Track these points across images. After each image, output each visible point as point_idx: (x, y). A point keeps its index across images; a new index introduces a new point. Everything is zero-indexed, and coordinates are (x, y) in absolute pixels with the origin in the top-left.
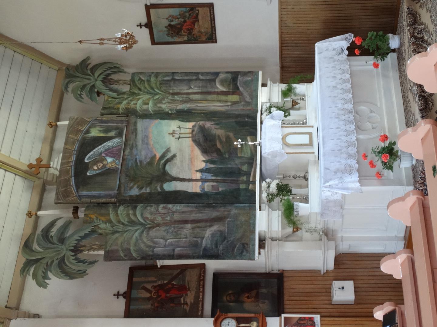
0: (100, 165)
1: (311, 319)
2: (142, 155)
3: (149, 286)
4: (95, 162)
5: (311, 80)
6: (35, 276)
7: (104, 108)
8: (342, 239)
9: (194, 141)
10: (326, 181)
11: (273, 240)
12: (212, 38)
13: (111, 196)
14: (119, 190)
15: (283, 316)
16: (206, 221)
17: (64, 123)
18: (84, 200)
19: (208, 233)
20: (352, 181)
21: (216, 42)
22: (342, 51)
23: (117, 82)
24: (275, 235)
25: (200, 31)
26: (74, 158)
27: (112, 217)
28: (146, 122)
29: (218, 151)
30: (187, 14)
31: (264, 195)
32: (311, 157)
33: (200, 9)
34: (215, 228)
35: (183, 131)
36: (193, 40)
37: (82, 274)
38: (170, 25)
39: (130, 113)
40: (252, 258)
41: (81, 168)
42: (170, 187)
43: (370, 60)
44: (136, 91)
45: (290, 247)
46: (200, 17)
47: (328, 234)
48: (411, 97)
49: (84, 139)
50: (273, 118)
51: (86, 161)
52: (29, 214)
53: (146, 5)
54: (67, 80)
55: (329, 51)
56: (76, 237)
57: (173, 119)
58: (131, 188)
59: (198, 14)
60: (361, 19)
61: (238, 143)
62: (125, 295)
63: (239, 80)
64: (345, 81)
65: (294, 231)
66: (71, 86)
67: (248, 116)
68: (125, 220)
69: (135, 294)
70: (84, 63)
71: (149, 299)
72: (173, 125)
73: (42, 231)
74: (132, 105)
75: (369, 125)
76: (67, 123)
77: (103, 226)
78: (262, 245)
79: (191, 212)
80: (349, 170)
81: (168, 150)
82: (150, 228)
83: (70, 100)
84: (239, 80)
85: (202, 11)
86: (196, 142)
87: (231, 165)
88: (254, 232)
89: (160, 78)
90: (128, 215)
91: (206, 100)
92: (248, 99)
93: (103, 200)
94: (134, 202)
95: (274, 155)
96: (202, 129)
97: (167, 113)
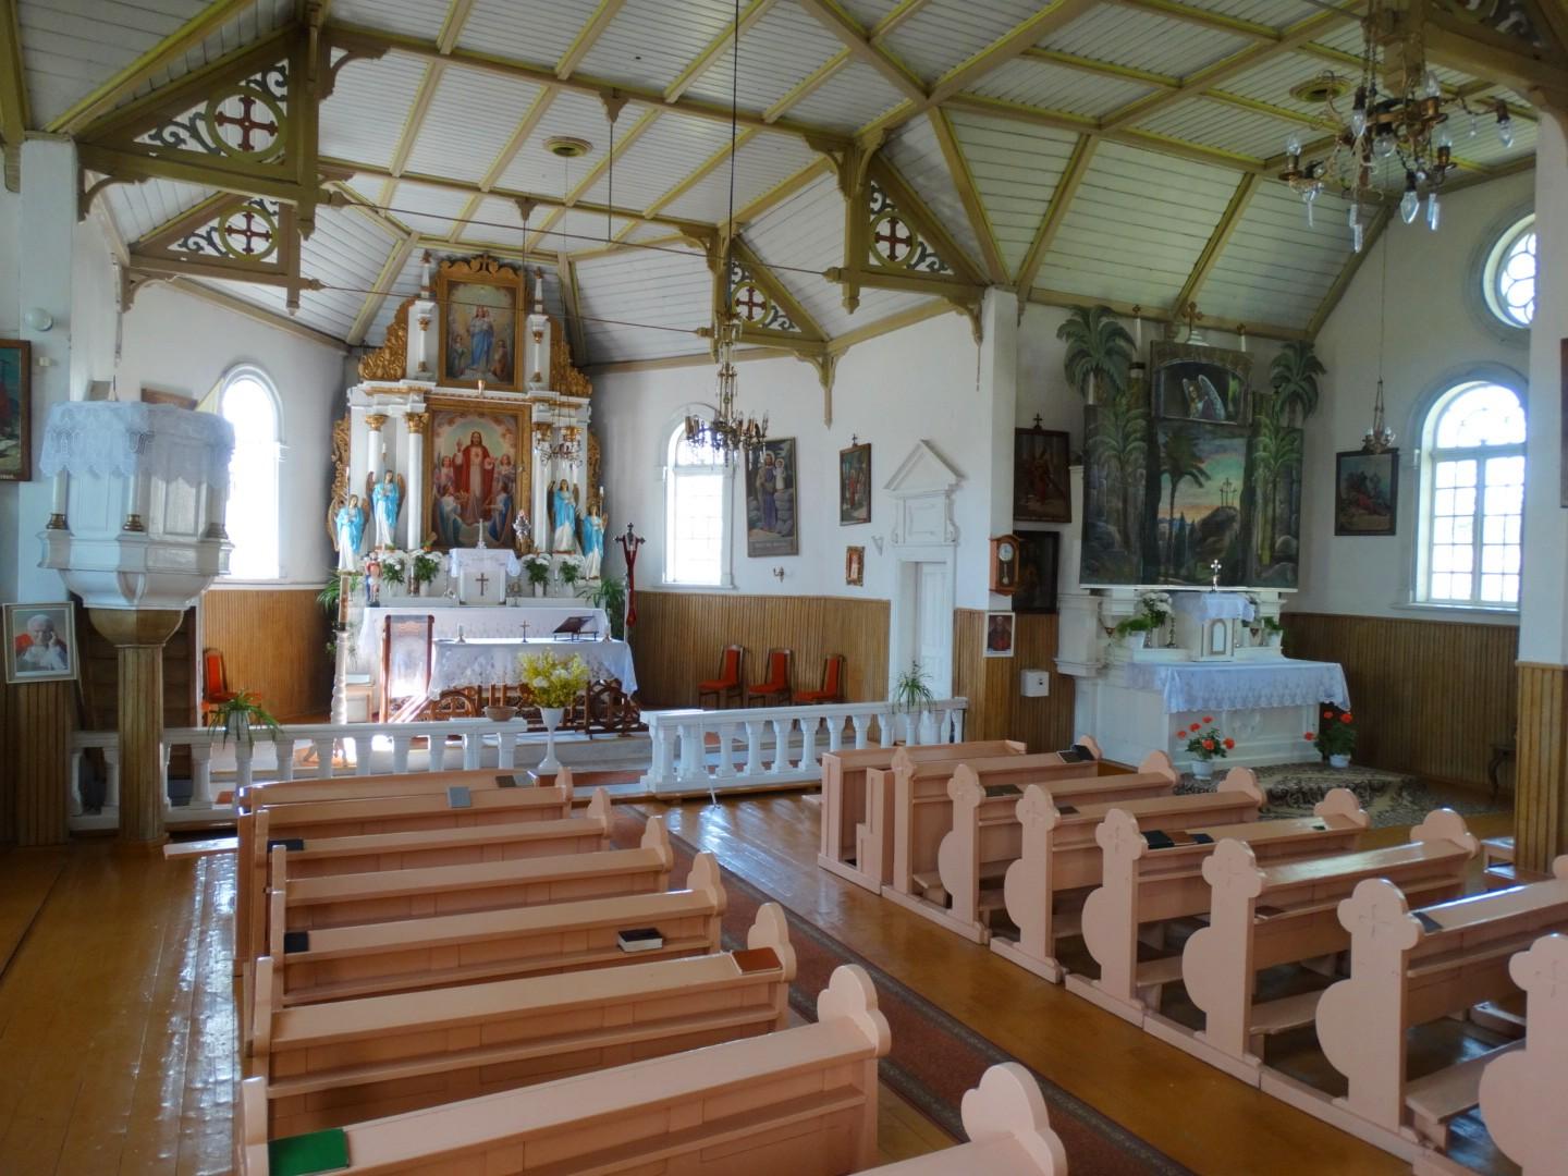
0: (1194, 395)
1: (1008, 647)
2: (1204, 446)
3: (1047, 456)
4: (1198, 388)
5: (1287, 652)
6: (1070, 322)
7: (1262, 396)
8: (1096, 685)
9: (1218, 509)
10: (1179, 673)
11: (1100, 604)
12: (1342, 529)
13: (1157, 409)
14: (1165, 419)
15: (1013, 614)
16: (1125, 527)
17: (1243, 344)
18: (1154, 376)
19: (1112, 529)
20: (1178, 704)
21: (1336, 534)
22: (1330, 696)
23: (1293, 411)
24: (1104, 606)
25: (1353, 515)
26: (1204, 361)
27: (1134, 412)
28: (1243, 449)
29: (1204, 539)
30: (1380, 501)
31: (1153, 596)
32: (1195, 652)
33: (1388, 517)
34: (1117, 537)
35: (1230, 495)
36: (1342, 506)
37: (1071, 378)
38: (1365, 478)
39: (1255, 429)
40: (1082, 580)
41: (1192, 370)
42: (1166, 480)
43: (1314, 730)
44: (1280, 436)
45: (1091, 624)
46: (1376, 517)
47: (1104, 669)
48: (1279, 777)
49: (1226, 372)
50: (1246, 606)
51: (1200, 377)
52: (1137, 308)
53: (1397, 449)
54: (1298, 346)
55: (1328, 680)
56: (1112, 370)
57: (1245, 483)
58: (1166, 434)
59: (1380, 514)
60: (1539, 782)
61: (1216, 565)
62: (1038, 427)
63: (1286, 565)
64: (1293, 697)
65: (1107, 629)
66: (1290, 352)
67: (1244, 576)
68: (1129, 429)
69: (1039, 440)
70: (1316, 366)
71: (1034, 458)
72: (1237, 484)
73: (1122, 329)
74: (1265, 431)
75: (1237, 724)
76: (1244, 349)
77: (1124, 401)
78: (1094, 592)
79: (1136, 508)
80: (1190, 700)
81: (1208, 478)
82: (1120, 459)
83: (1274, 350)
84: (1286, 565)
85: (1384, 519)
86: (1218, 511)
87: (1188, 554)
88: (1112, 582)
89: (1295, 464)
90: (1135, 431)
91: (1266, 522)
92: (1264, 575)
93: (1153, 400)
94: (1150, 439)
95: (1203, 610)
96: (1232, 519)
97: (1252, 475)
